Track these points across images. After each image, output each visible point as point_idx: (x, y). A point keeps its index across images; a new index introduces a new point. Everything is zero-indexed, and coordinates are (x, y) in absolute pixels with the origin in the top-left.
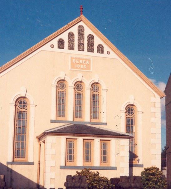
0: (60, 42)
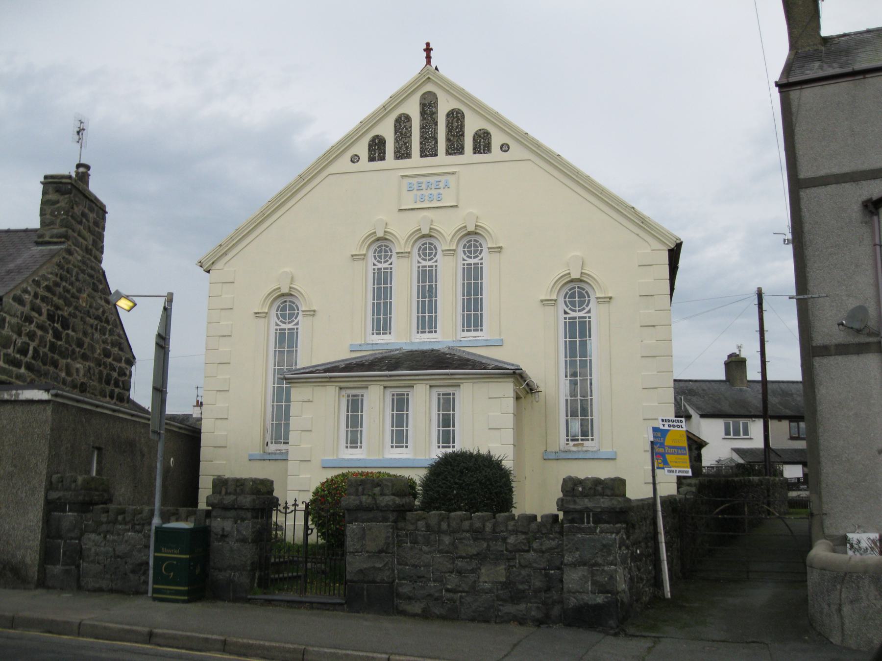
0: (376, 144)
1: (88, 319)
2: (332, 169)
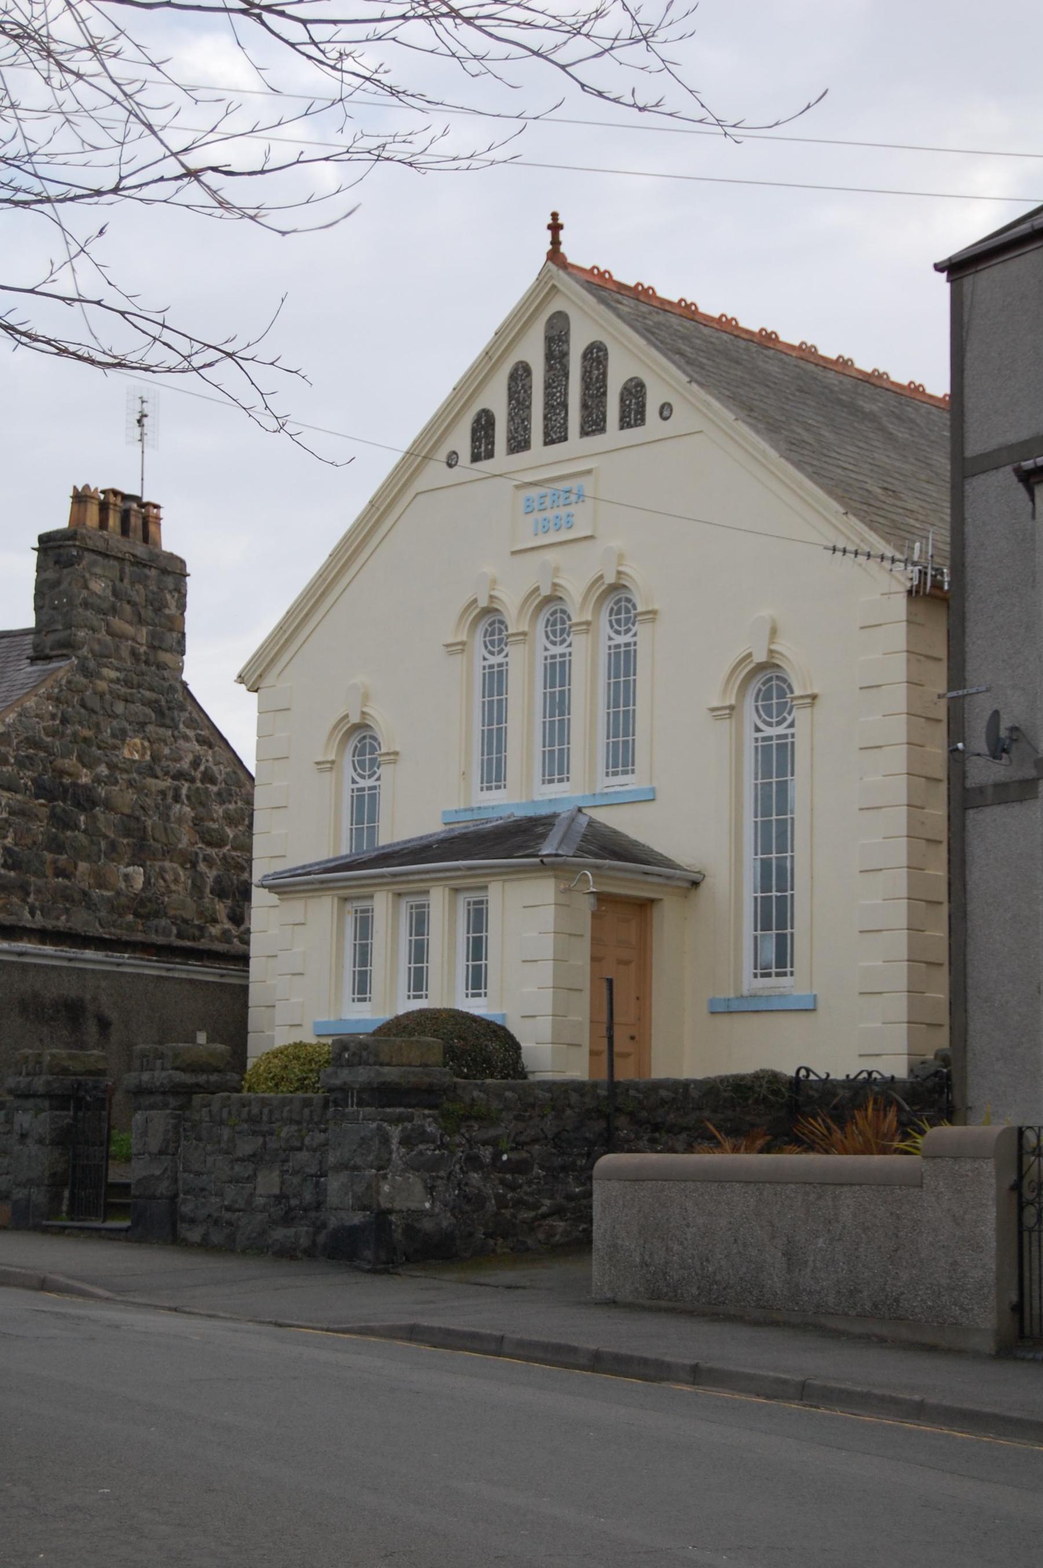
1: (150, 781)
2: (421, 483)
